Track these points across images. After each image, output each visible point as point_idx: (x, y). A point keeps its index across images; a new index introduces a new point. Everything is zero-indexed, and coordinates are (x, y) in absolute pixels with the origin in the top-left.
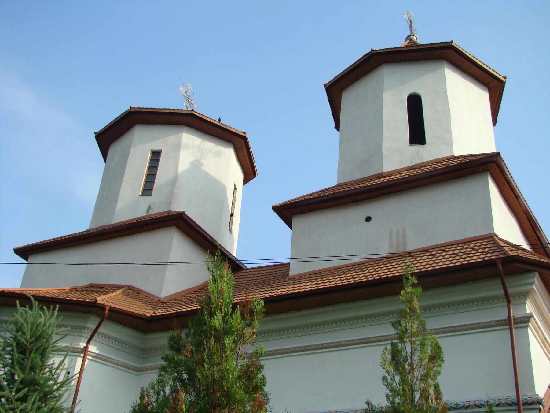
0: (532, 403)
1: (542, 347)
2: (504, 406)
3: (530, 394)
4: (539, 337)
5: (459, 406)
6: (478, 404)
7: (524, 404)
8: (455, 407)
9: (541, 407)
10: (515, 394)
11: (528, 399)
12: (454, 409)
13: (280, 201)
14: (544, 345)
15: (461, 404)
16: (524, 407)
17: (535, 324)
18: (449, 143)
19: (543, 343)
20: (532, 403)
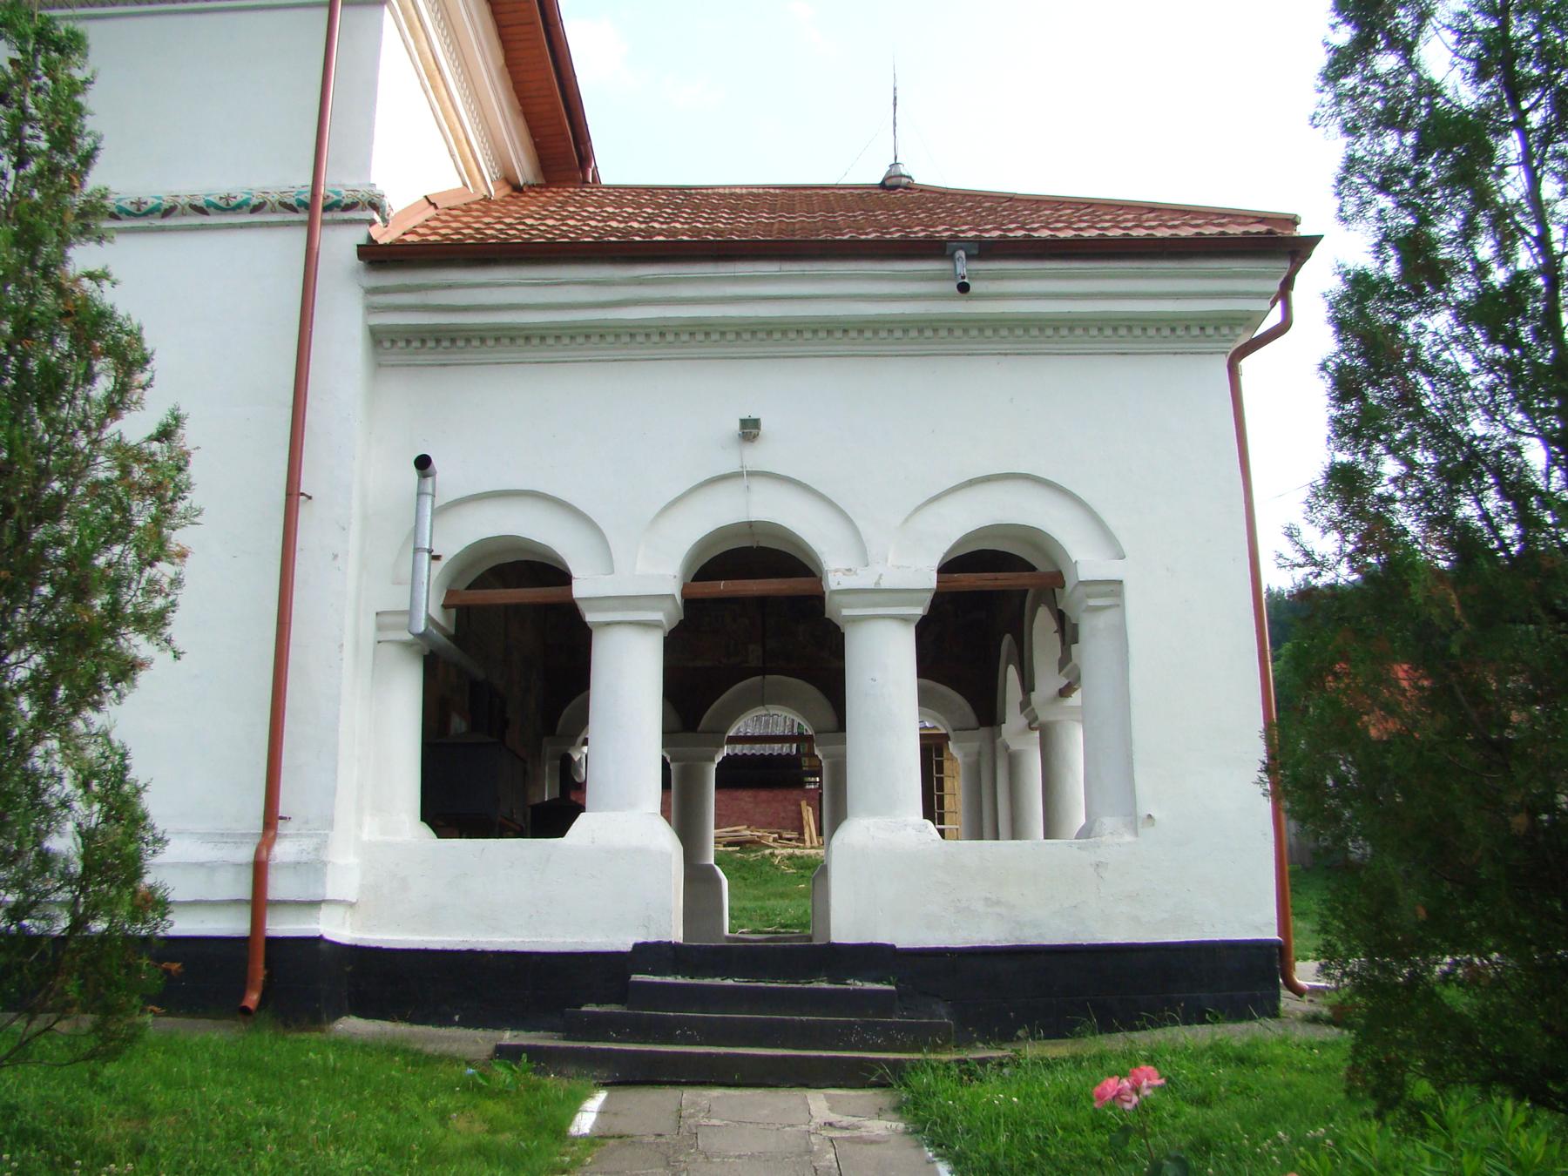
0: (351, 206)
1: (452, 156)
2: (274, 211)
3: (352, 183)
4: (421, 54)
5: (145, 208)
6: (200, 203)
7: (327, 209)
8: (132, 209)
9: (377, 217)
10: (310, 182)
11: (344, 193)
12: (130, 214)
13: (1317, 252)
14: (434, 87)
15: (152, 202)
16: (328, 216)
17: (413, 12)
18: (366, 168)
19: (430, 77)
20: (351, 206)
